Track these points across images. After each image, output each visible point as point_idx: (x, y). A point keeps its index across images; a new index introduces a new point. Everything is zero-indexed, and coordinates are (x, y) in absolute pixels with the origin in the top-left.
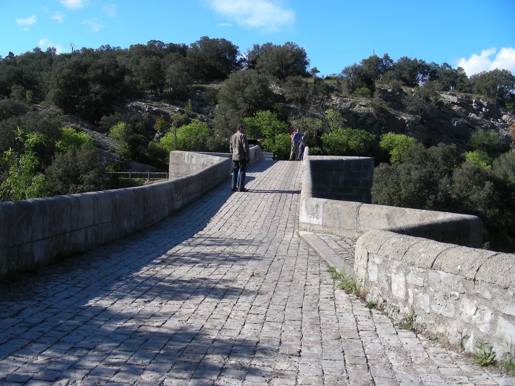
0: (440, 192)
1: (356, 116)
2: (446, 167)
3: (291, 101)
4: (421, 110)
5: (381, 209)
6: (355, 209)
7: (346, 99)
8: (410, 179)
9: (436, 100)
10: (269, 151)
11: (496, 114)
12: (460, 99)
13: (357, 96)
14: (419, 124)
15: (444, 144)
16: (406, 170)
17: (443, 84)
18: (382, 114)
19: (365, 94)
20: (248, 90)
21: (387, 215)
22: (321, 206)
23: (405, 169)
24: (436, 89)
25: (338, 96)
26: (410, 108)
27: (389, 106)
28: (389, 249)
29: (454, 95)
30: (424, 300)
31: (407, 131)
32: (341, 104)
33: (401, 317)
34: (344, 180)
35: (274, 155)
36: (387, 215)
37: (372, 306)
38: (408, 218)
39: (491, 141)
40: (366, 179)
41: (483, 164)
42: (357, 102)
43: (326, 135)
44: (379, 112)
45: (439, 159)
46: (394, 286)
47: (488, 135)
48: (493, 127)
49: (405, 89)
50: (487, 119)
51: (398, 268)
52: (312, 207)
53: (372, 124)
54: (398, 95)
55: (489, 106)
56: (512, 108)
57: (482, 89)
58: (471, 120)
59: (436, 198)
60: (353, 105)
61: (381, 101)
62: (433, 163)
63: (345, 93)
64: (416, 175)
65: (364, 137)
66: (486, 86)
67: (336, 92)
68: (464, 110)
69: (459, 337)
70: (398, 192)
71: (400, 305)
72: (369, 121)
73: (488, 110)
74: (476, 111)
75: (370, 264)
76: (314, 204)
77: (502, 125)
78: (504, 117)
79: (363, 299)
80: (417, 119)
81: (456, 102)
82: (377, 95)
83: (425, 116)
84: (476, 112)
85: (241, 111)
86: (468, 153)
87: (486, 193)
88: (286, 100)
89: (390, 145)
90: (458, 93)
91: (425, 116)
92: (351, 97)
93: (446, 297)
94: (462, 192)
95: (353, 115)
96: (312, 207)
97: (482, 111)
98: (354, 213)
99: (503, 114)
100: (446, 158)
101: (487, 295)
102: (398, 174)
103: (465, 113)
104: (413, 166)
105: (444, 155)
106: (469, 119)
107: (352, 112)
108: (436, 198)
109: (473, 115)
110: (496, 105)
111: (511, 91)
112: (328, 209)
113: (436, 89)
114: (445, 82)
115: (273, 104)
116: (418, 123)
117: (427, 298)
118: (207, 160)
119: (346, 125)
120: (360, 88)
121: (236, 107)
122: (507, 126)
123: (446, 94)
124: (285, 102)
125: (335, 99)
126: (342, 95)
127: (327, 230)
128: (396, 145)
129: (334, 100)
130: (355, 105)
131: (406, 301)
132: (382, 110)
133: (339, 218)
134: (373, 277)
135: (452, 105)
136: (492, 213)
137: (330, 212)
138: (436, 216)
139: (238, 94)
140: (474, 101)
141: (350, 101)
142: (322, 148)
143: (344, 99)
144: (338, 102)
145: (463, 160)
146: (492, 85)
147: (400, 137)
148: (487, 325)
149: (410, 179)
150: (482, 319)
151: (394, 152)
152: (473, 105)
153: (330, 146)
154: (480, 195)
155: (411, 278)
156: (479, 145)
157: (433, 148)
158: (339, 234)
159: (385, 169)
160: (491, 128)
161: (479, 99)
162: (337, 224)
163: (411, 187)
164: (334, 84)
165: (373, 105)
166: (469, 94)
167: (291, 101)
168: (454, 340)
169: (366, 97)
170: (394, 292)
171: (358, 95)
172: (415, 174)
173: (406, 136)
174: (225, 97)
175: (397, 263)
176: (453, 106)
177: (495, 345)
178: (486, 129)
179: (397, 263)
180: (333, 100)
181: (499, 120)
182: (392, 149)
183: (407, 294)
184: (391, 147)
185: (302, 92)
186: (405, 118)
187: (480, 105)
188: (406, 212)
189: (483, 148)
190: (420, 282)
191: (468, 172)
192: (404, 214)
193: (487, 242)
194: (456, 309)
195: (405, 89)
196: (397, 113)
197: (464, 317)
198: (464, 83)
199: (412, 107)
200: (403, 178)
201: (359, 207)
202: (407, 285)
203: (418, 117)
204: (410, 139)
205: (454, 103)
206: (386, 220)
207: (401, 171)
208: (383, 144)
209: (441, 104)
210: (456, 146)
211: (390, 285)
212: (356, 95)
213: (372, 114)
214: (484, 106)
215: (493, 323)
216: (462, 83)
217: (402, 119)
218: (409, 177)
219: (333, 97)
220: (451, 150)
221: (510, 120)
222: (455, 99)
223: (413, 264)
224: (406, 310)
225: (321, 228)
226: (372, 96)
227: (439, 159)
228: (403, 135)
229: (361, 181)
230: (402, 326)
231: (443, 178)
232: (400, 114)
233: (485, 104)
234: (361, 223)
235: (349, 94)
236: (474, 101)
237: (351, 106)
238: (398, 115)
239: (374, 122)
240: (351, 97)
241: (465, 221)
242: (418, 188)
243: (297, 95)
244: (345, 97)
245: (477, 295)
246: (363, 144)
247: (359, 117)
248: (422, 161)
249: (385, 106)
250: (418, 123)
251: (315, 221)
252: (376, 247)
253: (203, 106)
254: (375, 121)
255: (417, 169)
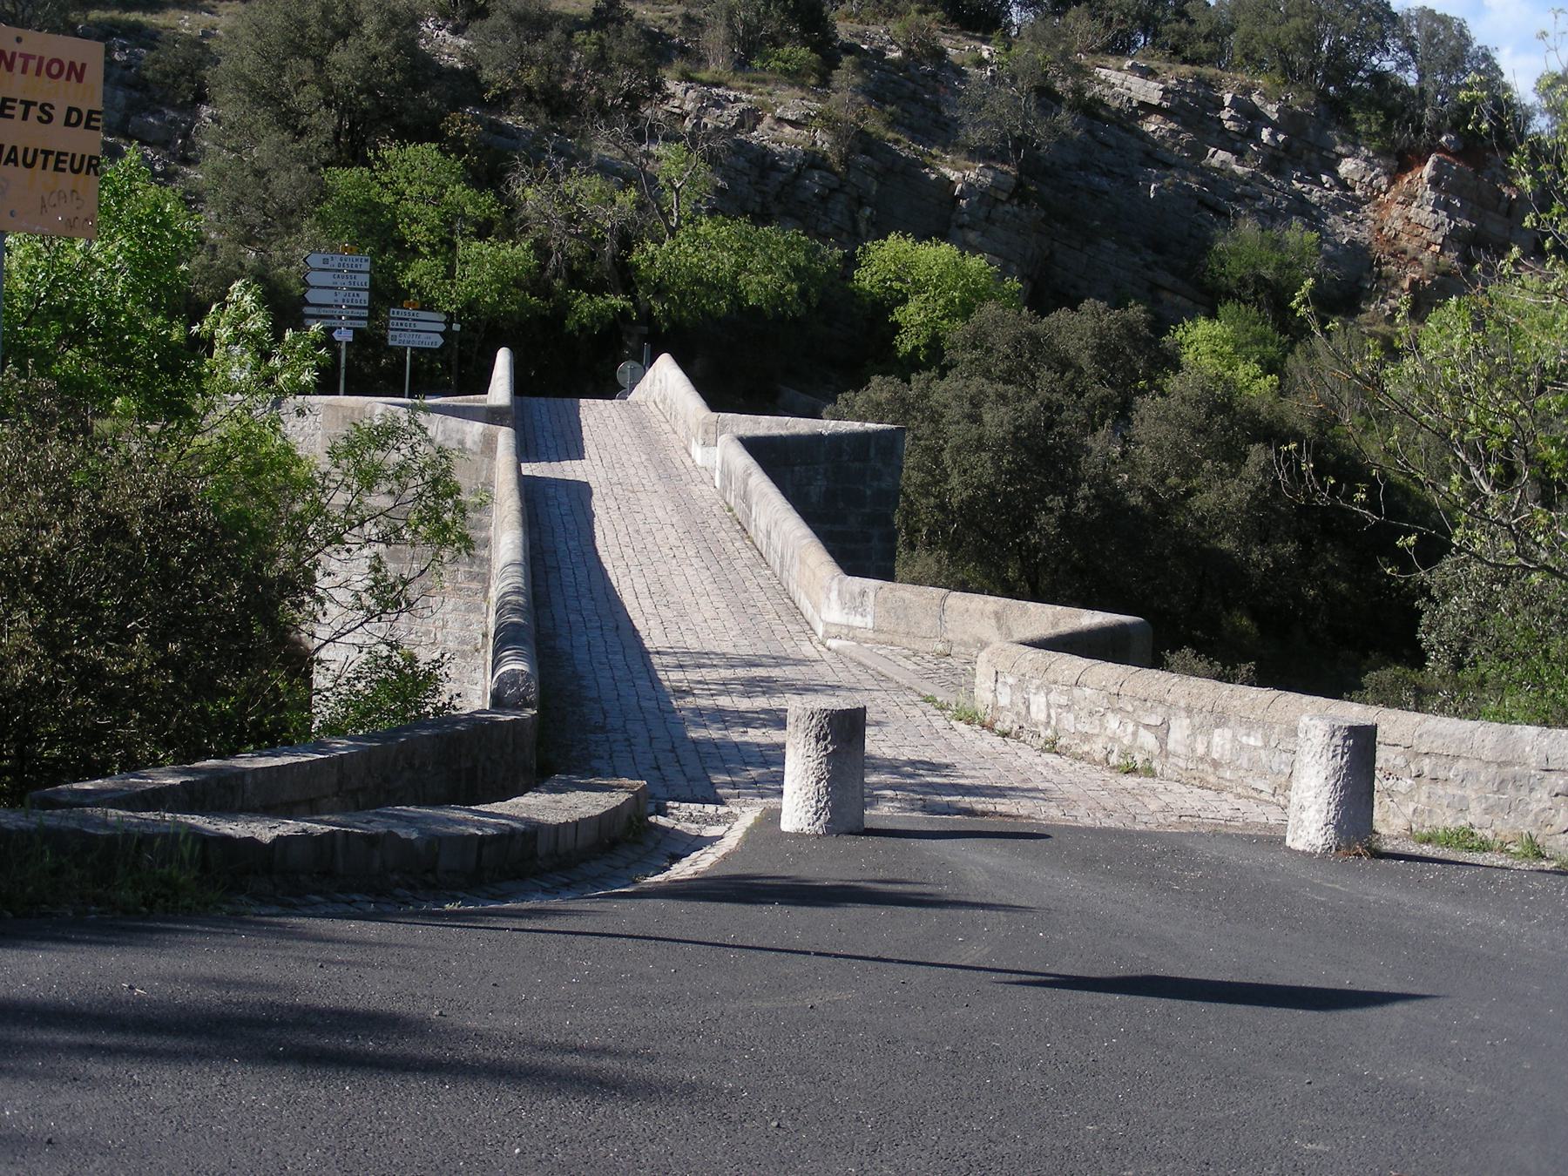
0: (1085, 486)
1: (763, 161)
2: (1108, 390)
3: (503, 101)
4: (1020, 142)
5: (986, 602)
6: (937, 601)
7: (720, 91)
8: (980, 438)
9: (1078, 91)
10: (430, 309)
11: (1314, 155)
12: (1173, 91)
13: (764, 82)
14: (1009, 200)
15: (1102, 305)
16: (967, 404)
17: (1108, 22)
18: (863, 159)
19: (797, 72)
20: (344, 57)
21: (996, 613)
22: (872, 595)
23: (958, 397)
24: (1076, 48)
25: (691, 80)
26: (975, 136)
27: (892, 124)
28: (1026, 667)
29: (1148, 73)
30: (1068, 721)
31: (961, 227)
32: (701, 112)
33: (1042, 742)
34: (823, 489)
35: (449, 323)
36: (996, 613)
37: (1005, 735)
38: (1033, 618)
39: (1290, 265)
40: (883, 485)
41: (1245, 371)
42: (764, 106)
43: (651, 247)
44: (851, 150)
45: (1085, 360)
46: (1033, 708)
47: (1277, 245)
48: (1301, 206)
49: (958, 48)
50: (1276, 173)
51: (1037, 688)
52: (852, 595)
53: (823, 199)
54: (925, 75)
55: (1289, 121)
56: (1376, 133)
57: (1263, 52)
58: (1214, 180)
59: (1071, 504)
60: (751, 118)
61: (860, 105)
62: (1063, 374)
63: (716, 67)
64: (1001, 425)
65: (800, 257)
66: (1277, 40)
67: (679, 64)
68: (1186, 137)
69: (1105, 752)
70: (937, 483)
71: (1041, 728)
72: (814, 182)
73: (1281, 137)
74: (1233, 141)
75: (999, 685)
76: (857, 590)
77: (1334, 201)
78: (1346, 167)
79: (991, 729)
80: (1001, 178)
81: (1155, 102)
82: (845, 76)
83: (1034, 168)
84: (1235, 144)
85: (311, 141)
86: (1196, 326)
87: (1250, 486)
88: (487, 96)
89: (896, 285)
90: (1165, 66)
91: (1034, 168)
92: (741, 84)
93: (1091, 714)
94: (1162, 479)
95: (749, 161)
96: (852, 595)
97: (1259, 142)
98: (935, 608)
99: (1341, 156)
100: (1106, 353)
101: (1130, 708)
102: (935, 418)
103: (1190, 147)
104: (990, 391)
105: (1100, 346)
106: (1204, 173)
107: (743, 146)
108: (1071, 504)
109: (1222, 155)
110: (1317, 115)
111: (1375, 60)
112: (885, 600)
113: (1076, 48)
114: (1116, 15)
115: (442, 117)
116: (1003, 197)
117: (1071, 717)
118: (444, 432)
119: (725, 204)
120: (777, 45)
121: (291, 122)
122: (1356, 204)
123: (1120, 70)
124: (480, 103)
125: (680, 94)
126: (704, 76)
127: (882, 637)
128: (919, 288)
129: (673, 96)
130: (759, 120)
131: (1049, 723)
132: (865, 142)
133: (906, 616)
134: (1004, 700)
135: (1140, 113)
136: (1268, 559)
137: (889, 605)
138: (1078, 617)
139: (300, 73)
140: (1228, 98)
141: (737, 99)
142: (633, 299)
143: (715, 90)
144: (688, 107)
145: (1172, 362)
146: (1300, 39)
147: (935, 255)
148: (1130, 737)
149: (980, 438)
150: (1125, 731)
151: (911, 314)
152: (1225, 115)
153: (668, 290)
154: (1228, 495)
155: (1053, 697)
156: (1243, 283)
157: (1062, 316)
158: (906, 645)
159: (888, 402)
160: (1290, 212)
161: (1248, 90)
162: (902, 628)
163: (984, 467)
164: (670, 20)
165: (829, 122)
166: (1208, 71)
167: (503, 101)
168: (1099, 756)
169: (802, 86)
170: (1033, 715)
171: (768, 76)
172: (996, 421)
173: (955, 251)
174: (244, 77)
175: (1036, 682)
176: (1143, 117)
177: (1136, 754)
178: (1270, 216)
179: (1036, 682)
180: (667, 97)
181: (1324, 178)
182: (904, 300)
183: (1049, 716)
184: (900, 291)
185: (550, 64)
186: (954, 175)
187: (1251, 116)
188: (1028, 609)
189: (1256, 293)
190: (1063, 700)
191: (1186, 410)
192: (1025, 612)
193: (1246, 662)
194: (1101, 725)
195: (958, 48)
196: (922, 154)
197: (1108, 732)
198: (1191, 22)
199: (980, 132)
200: (957, 431)
201: (944, 598)
202: (1048, 706)
203: (1007, 173)
204: (975, 263)
205: (1148, 108)
206: (993, 622)
207: (945, 406)
208: (865, 279)
209: (1091, 110)
210: (1145, 312)
211: (1028, 708)
212: (760, 76)
213: (825, 158)
214: (1268, 123)
215: (1135, 734)
216: (1184, 25)
217: (943, 179)
218: (975, 431)
219: (672, 86)
220: (1130, 329)
221: (1367, 180)
222: (1151, 92)
223: (1055, 682)
224: (1049, 733)
225: (870, 635)
226: (825, 82)
227: (1085, 360)
228: (944, 247)
229: (869, 492)
230: (1043, 750)
231: (1095, 430)
232: (935, 157)
233: (1272, 111)
234: (949, 626)
235: (735, 70)
236: (1228, 98)
237: (741, 124)
238: (928, 160)
239: (832, 190)
240: (741, 84)
241: (1123, 626)
242: (1008, 472)
243: (532, 77)
244: (718, 85)
245: (1120, 709)
246: (795, 287)
247: (774, 166)
248: (1020, 364)
249: (874, 125)
250: (1003, 197)
251: (857, 621)
252: (1008, 664)
253: (145, 109)
254: (836, 185)
255: (1002, 397)
